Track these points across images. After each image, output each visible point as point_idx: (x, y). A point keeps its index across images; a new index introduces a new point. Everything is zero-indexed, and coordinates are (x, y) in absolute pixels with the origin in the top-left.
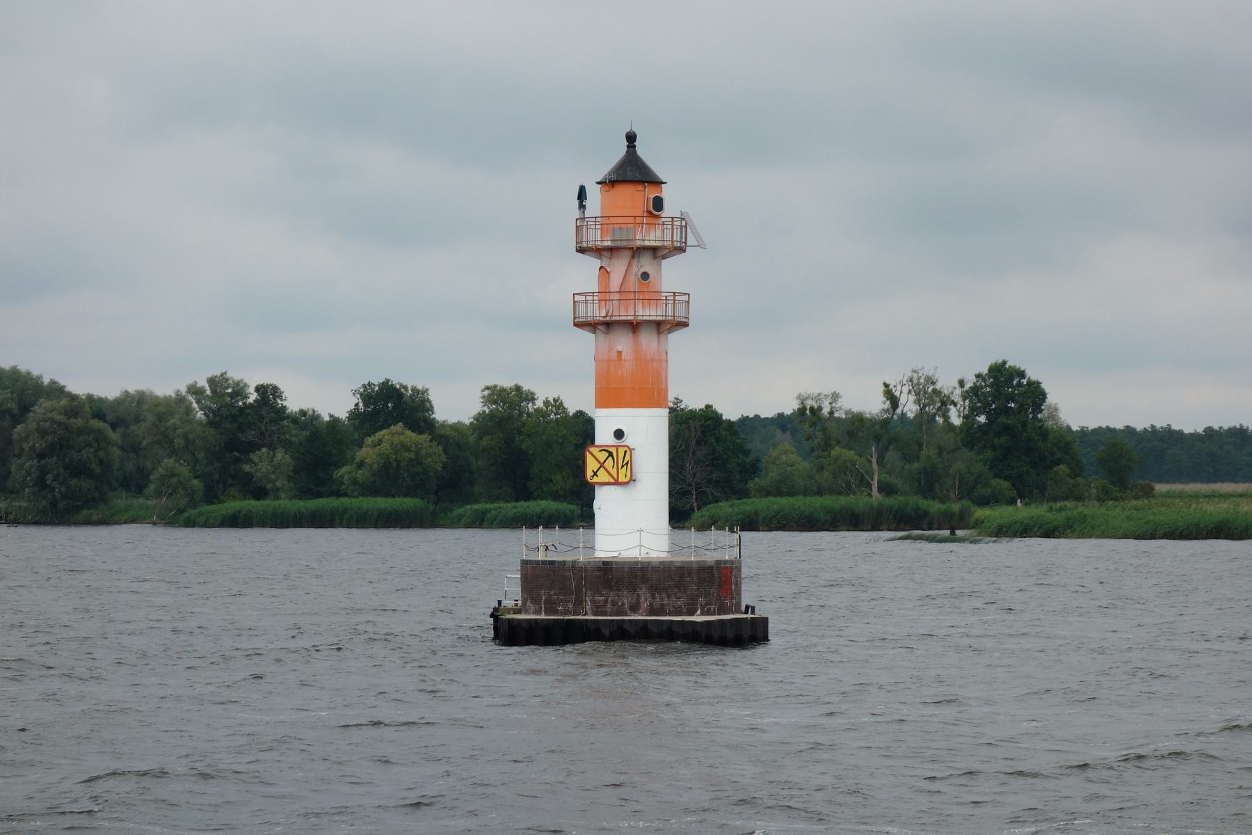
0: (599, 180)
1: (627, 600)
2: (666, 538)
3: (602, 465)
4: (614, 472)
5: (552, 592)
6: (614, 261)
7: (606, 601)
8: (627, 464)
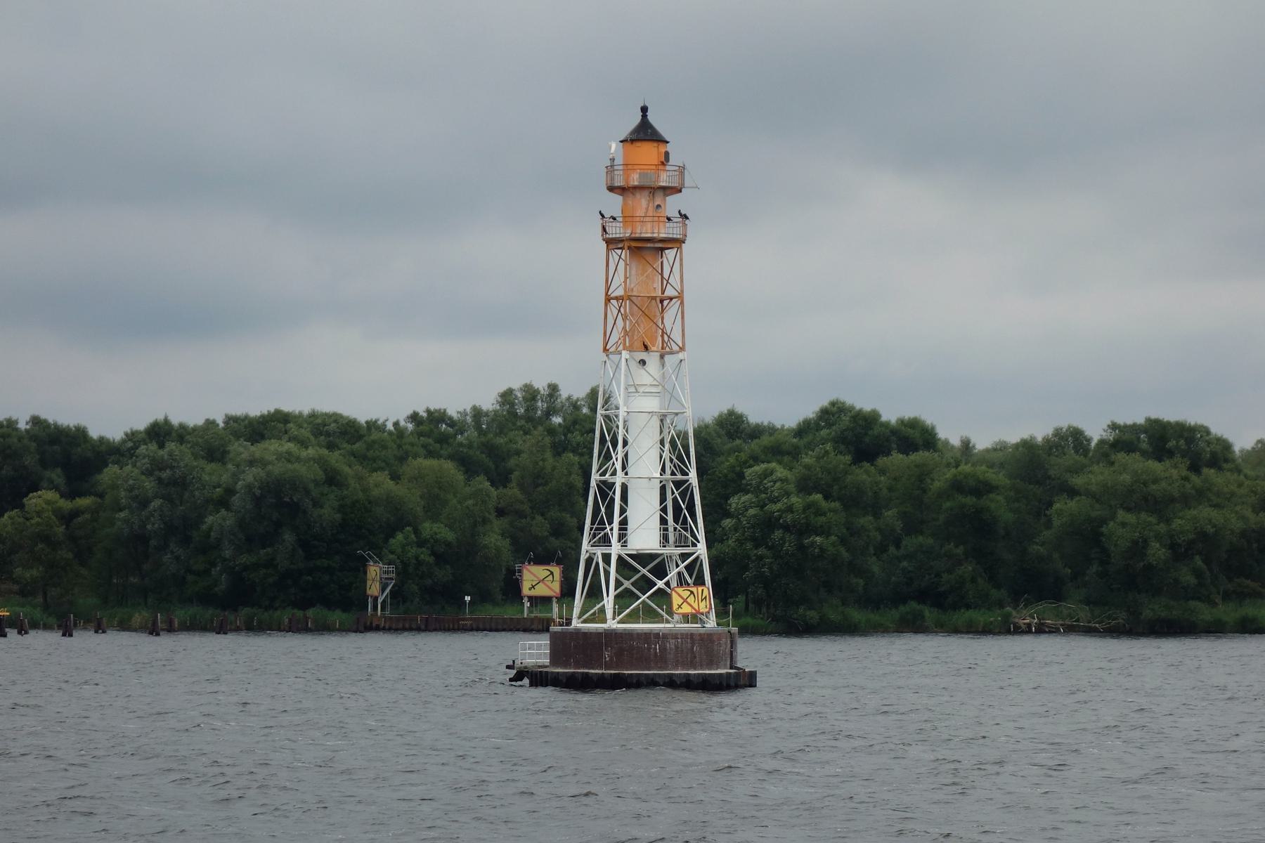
0: (622, 139)
3: (685, 601)
8: (705, 598)
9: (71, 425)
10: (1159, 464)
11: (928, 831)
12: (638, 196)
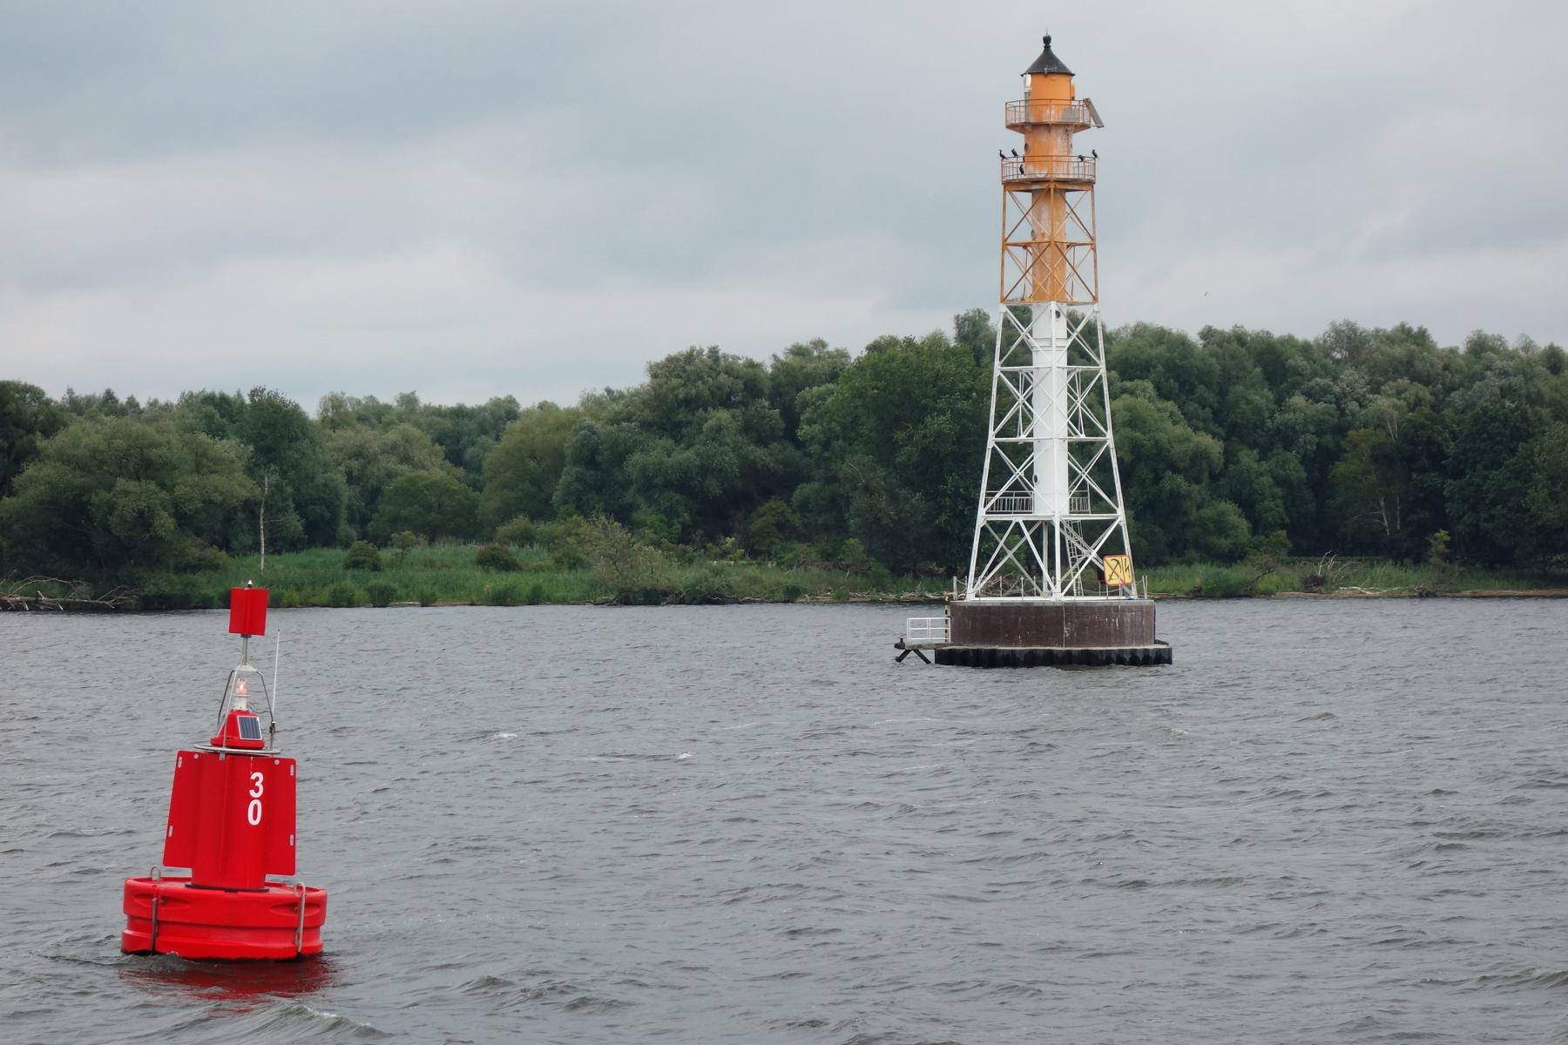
12: (1053, 133)
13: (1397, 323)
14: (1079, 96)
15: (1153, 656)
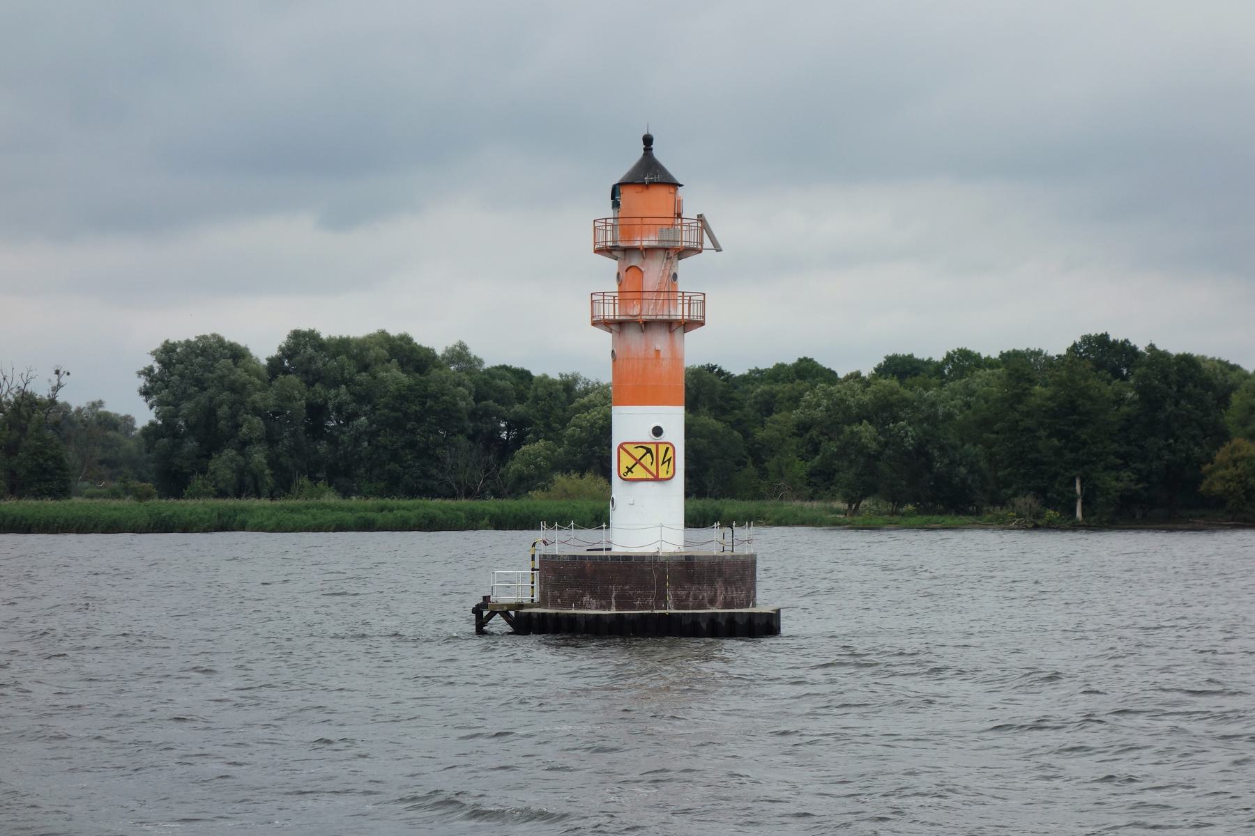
1: (706, 594)
2: (682, 533)
3: (638, 462)
4: (653, 469)
5: (627, 587)
6: (648, 261)
7: (688, 595)
8: (669, 460)
9: (226, 340)
10: (516, 502)
11: (379, 683)
13: (451, 343)
14: (689, 212)
15: (740, 622)
